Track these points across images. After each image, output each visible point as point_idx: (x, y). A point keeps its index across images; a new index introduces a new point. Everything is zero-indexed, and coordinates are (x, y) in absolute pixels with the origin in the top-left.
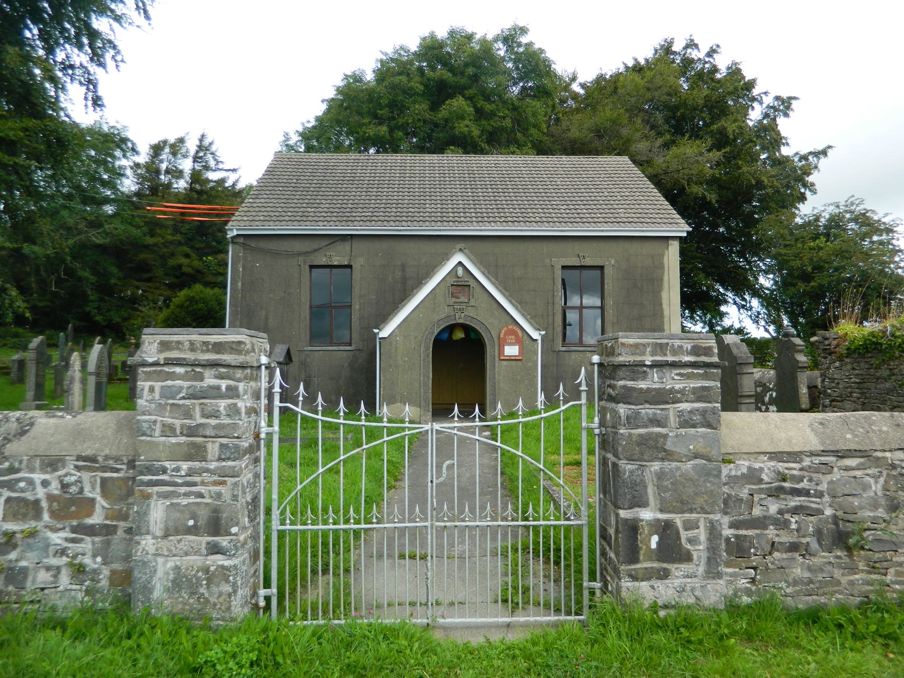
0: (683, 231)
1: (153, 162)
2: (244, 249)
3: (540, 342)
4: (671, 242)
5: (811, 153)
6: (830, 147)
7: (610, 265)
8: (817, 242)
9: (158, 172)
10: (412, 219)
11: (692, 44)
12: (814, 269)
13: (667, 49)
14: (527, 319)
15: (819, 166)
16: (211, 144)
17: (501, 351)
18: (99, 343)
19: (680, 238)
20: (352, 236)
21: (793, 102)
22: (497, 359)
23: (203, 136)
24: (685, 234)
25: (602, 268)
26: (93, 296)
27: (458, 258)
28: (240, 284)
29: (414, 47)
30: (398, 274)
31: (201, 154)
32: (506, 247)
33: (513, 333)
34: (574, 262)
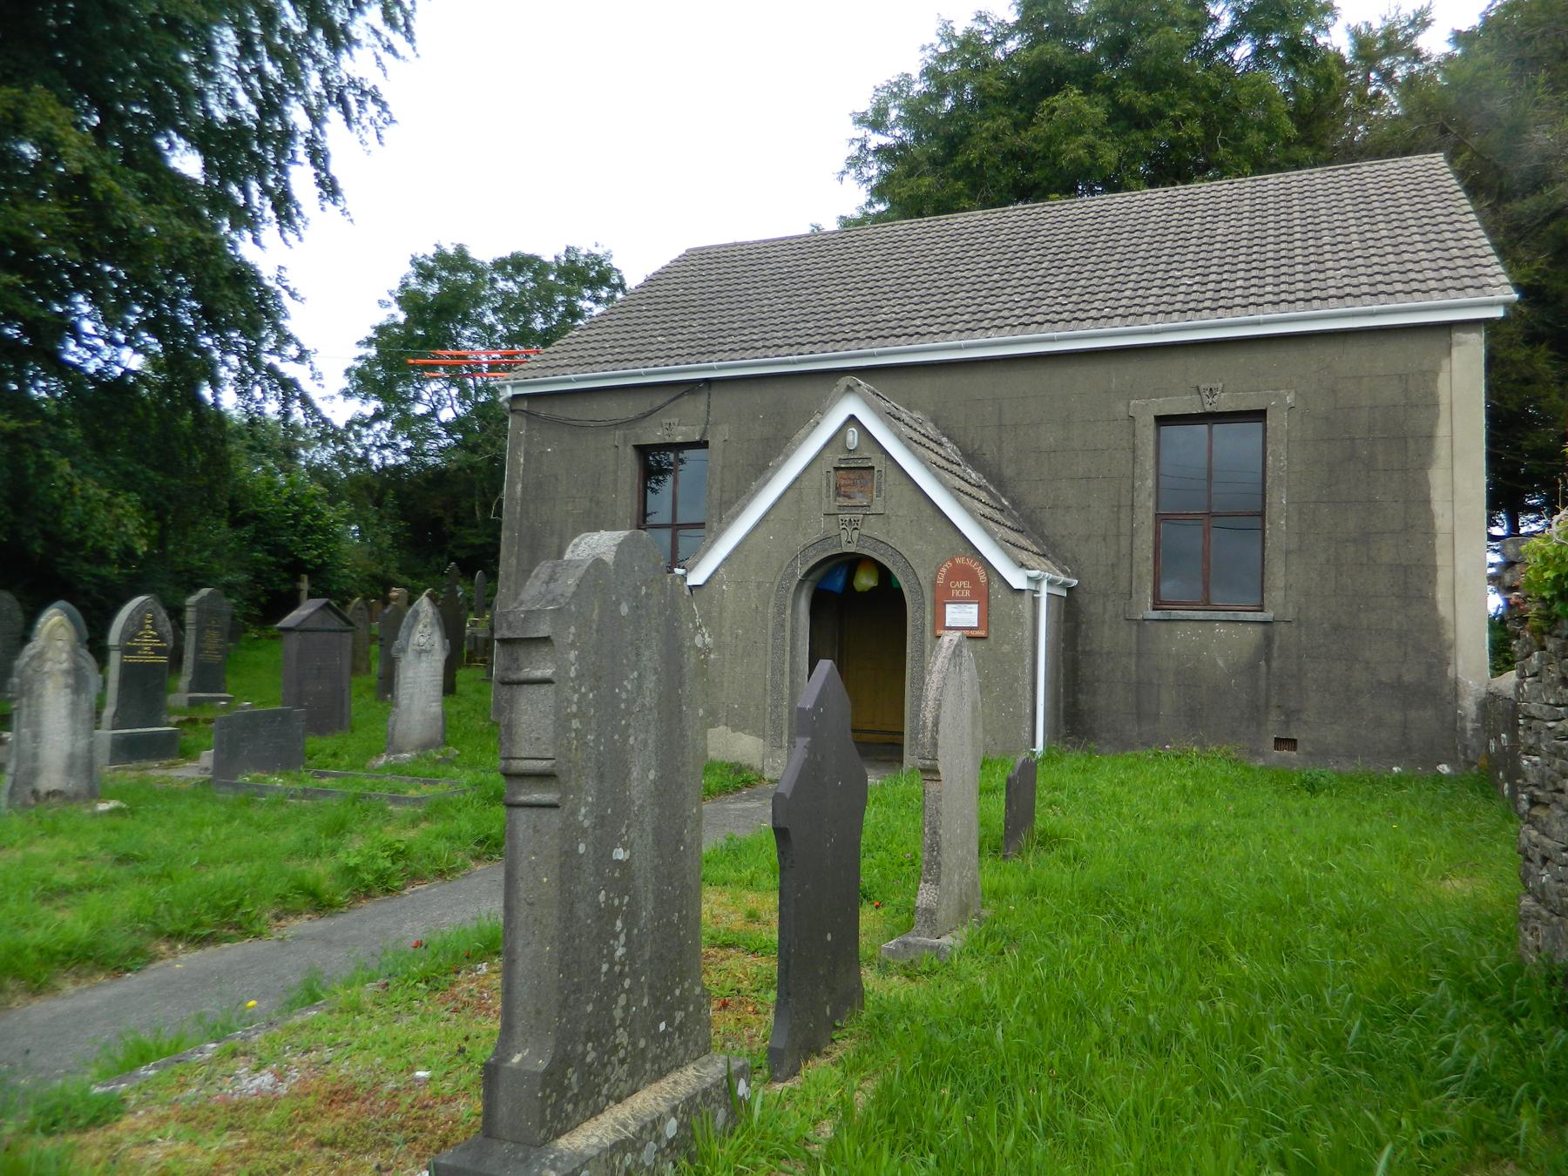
4: (1459, 336)
7: (1282, 402)
18: (311, 596)
20: (708, 382)
24: (1499, 313)
28: (519, 487)
32: (1021, 380)
33: (966, 574)
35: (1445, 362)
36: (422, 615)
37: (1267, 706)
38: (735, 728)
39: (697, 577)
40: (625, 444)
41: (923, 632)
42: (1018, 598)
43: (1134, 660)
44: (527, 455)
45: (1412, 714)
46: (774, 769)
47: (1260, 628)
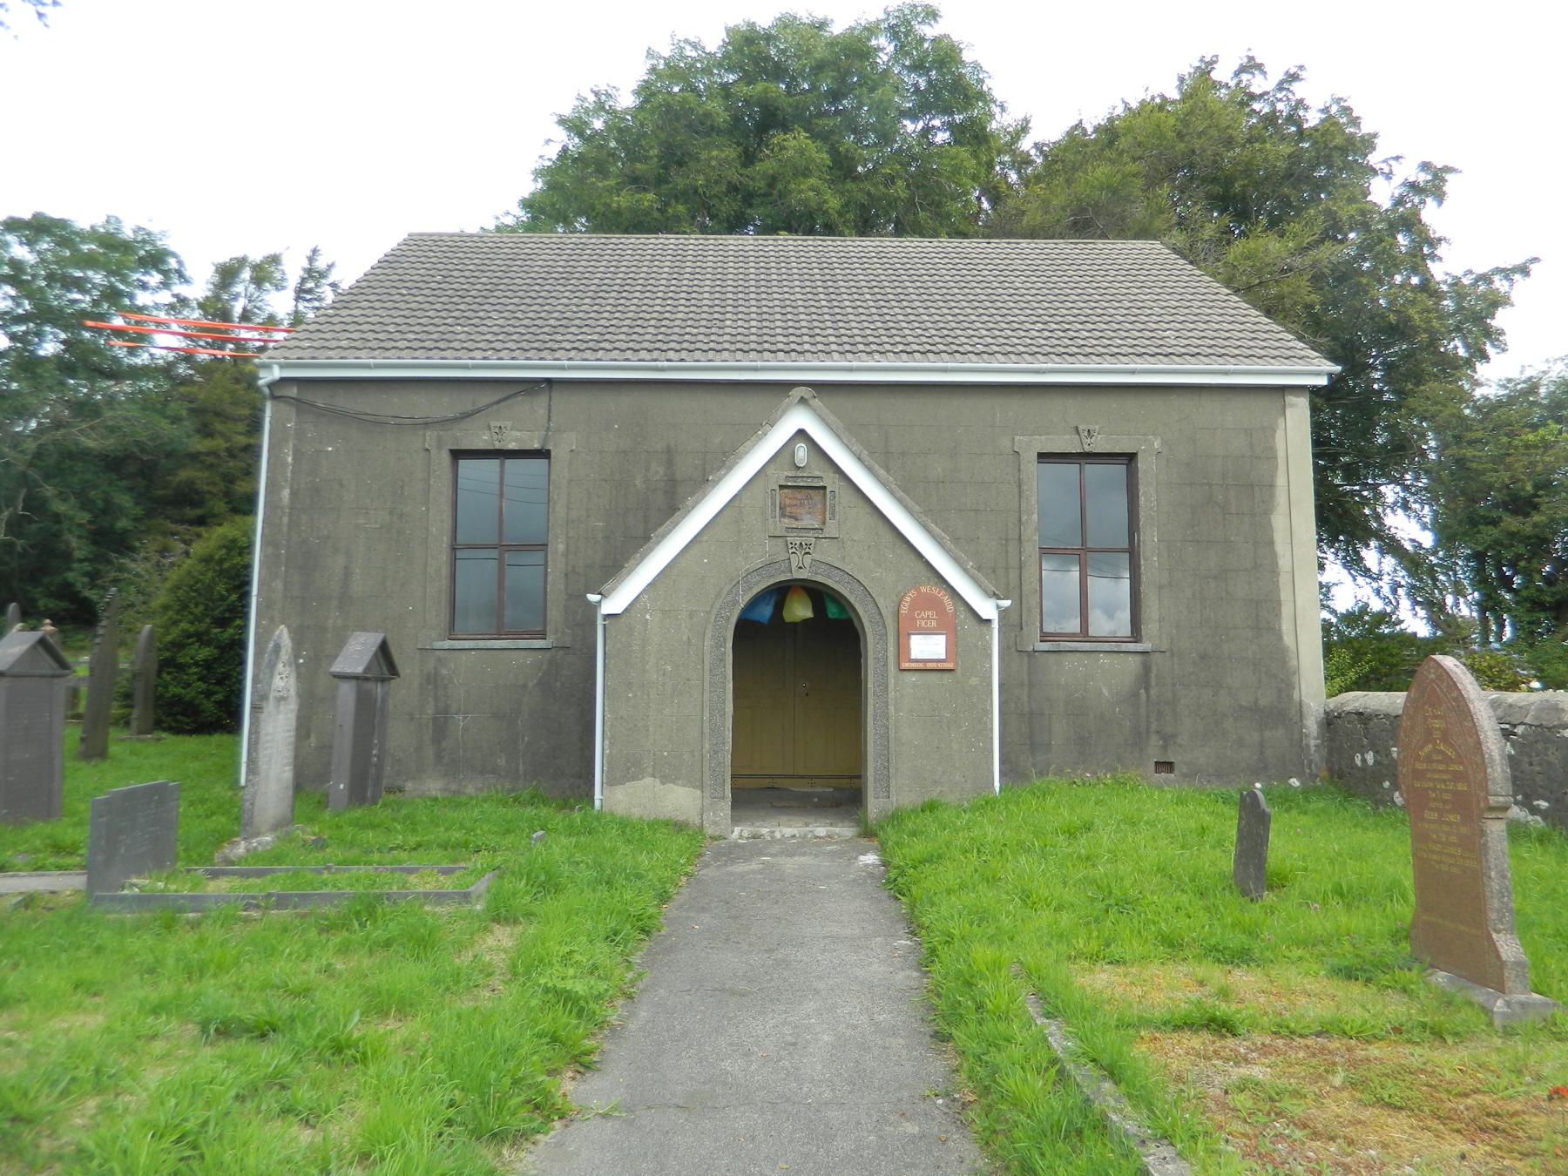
0: (1318, 374)
1: (217, 298)
2: (299, 412)
3: (995, 625)
4: (1290, 399)
5: (1498, 271)
6: (1535, 260)
8: (1541, 431)
9: (225, 315)
10: (692, 347)
11: (1252, 66)
12: (1537, 487)
13: (1204, 71)
14: (965, 570)
15: (1514, 297)
16: (330, 266)
17: (902, 648)
19: (1314, 391)
20: (549, 382)
21: (1448, 176)
22: (892, 667)
23: (315, 251)
24: (1323, 381)
25: (1130, 458)
26: (79, 547)
27: (798, 419)
28: (286, 493)
29: (714, 42)
30: (658, 471)
31: (310, 285)
34: (1068, 444)
35: (1281, 421)
36: (283, 651)
37: (1148, 731)
38: (665, 779)
39: (616, 603)
40: (439, 447)
41: (885, 665)
42: (984, 628)
43: (1026, 689)
44: (297, 454)
45: (1267, 734)
46: (715, 823)
47: (1138, 658)
